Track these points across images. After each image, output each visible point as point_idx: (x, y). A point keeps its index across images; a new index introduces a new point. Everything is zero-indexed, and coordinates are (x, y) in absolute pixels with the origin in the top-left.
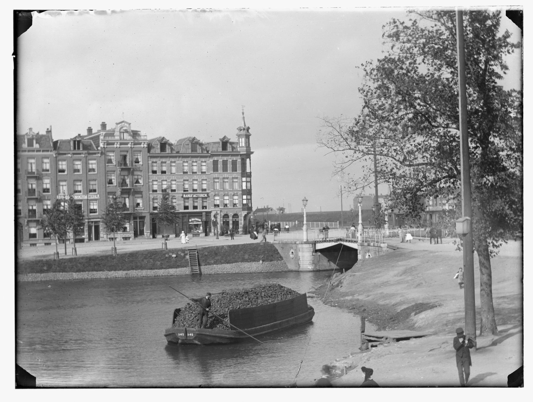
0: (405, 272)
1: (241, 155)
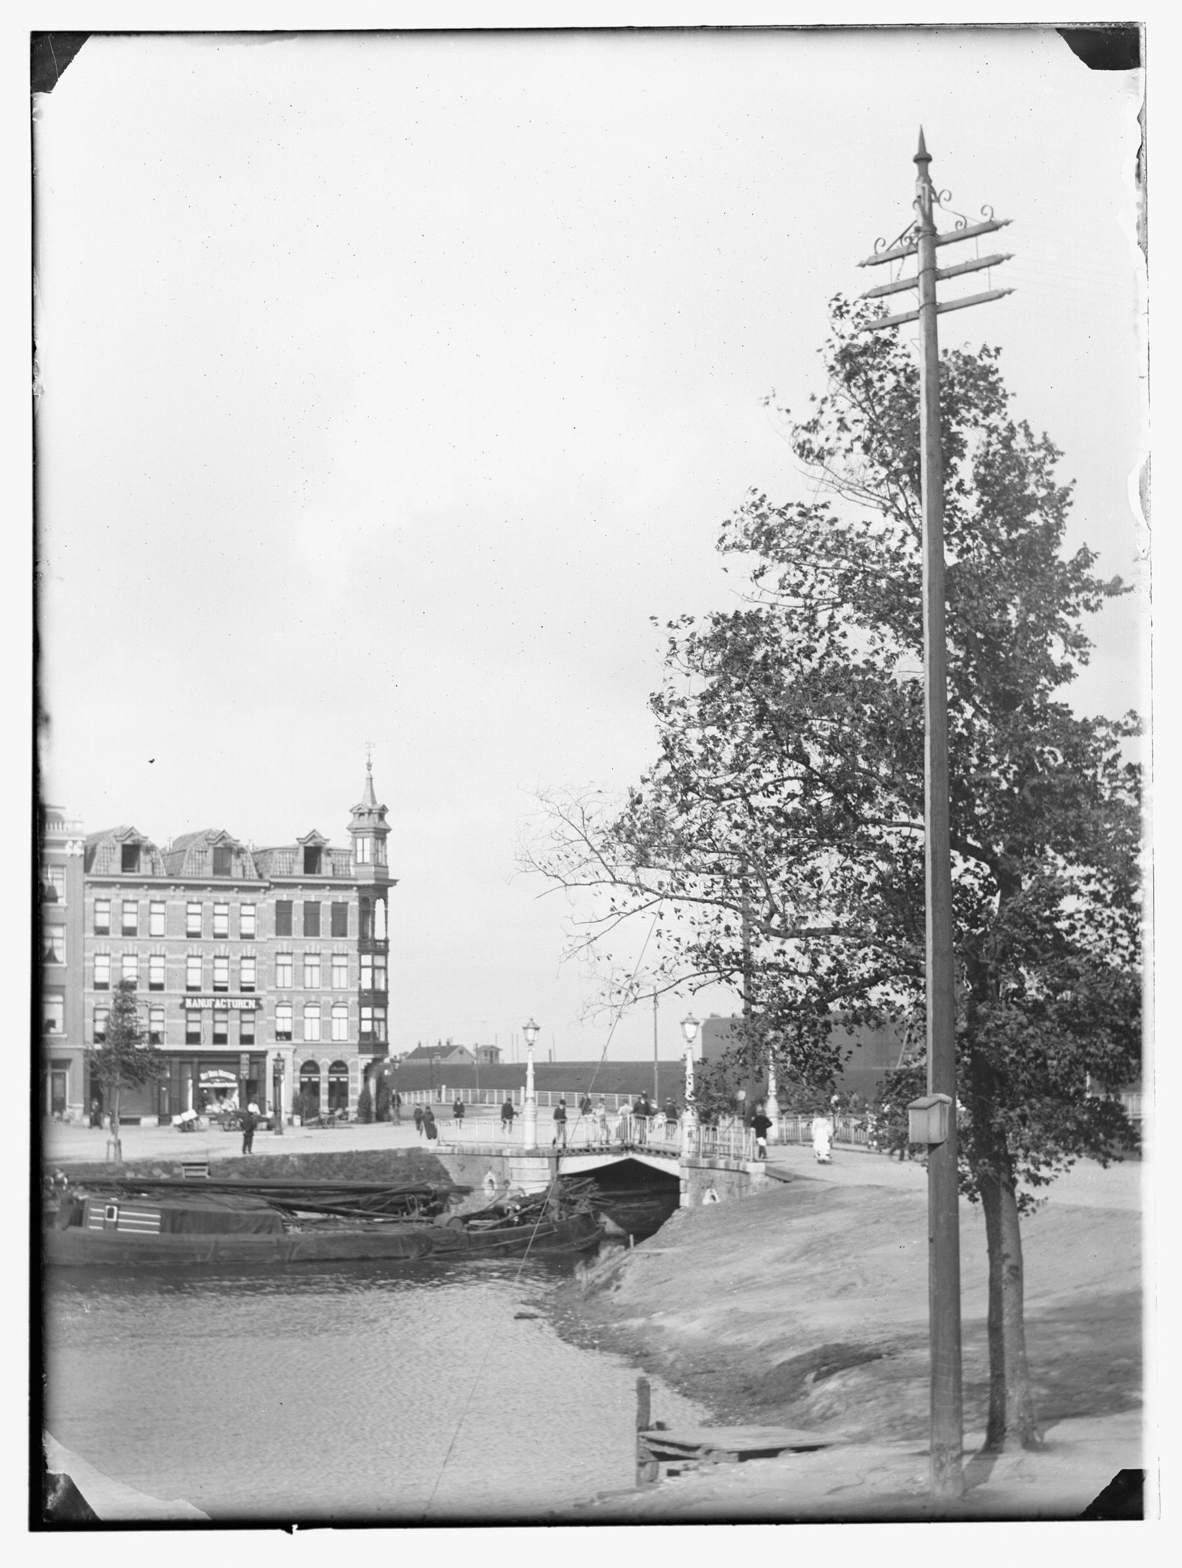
0: (807, 1251)
1: (359, 887)
